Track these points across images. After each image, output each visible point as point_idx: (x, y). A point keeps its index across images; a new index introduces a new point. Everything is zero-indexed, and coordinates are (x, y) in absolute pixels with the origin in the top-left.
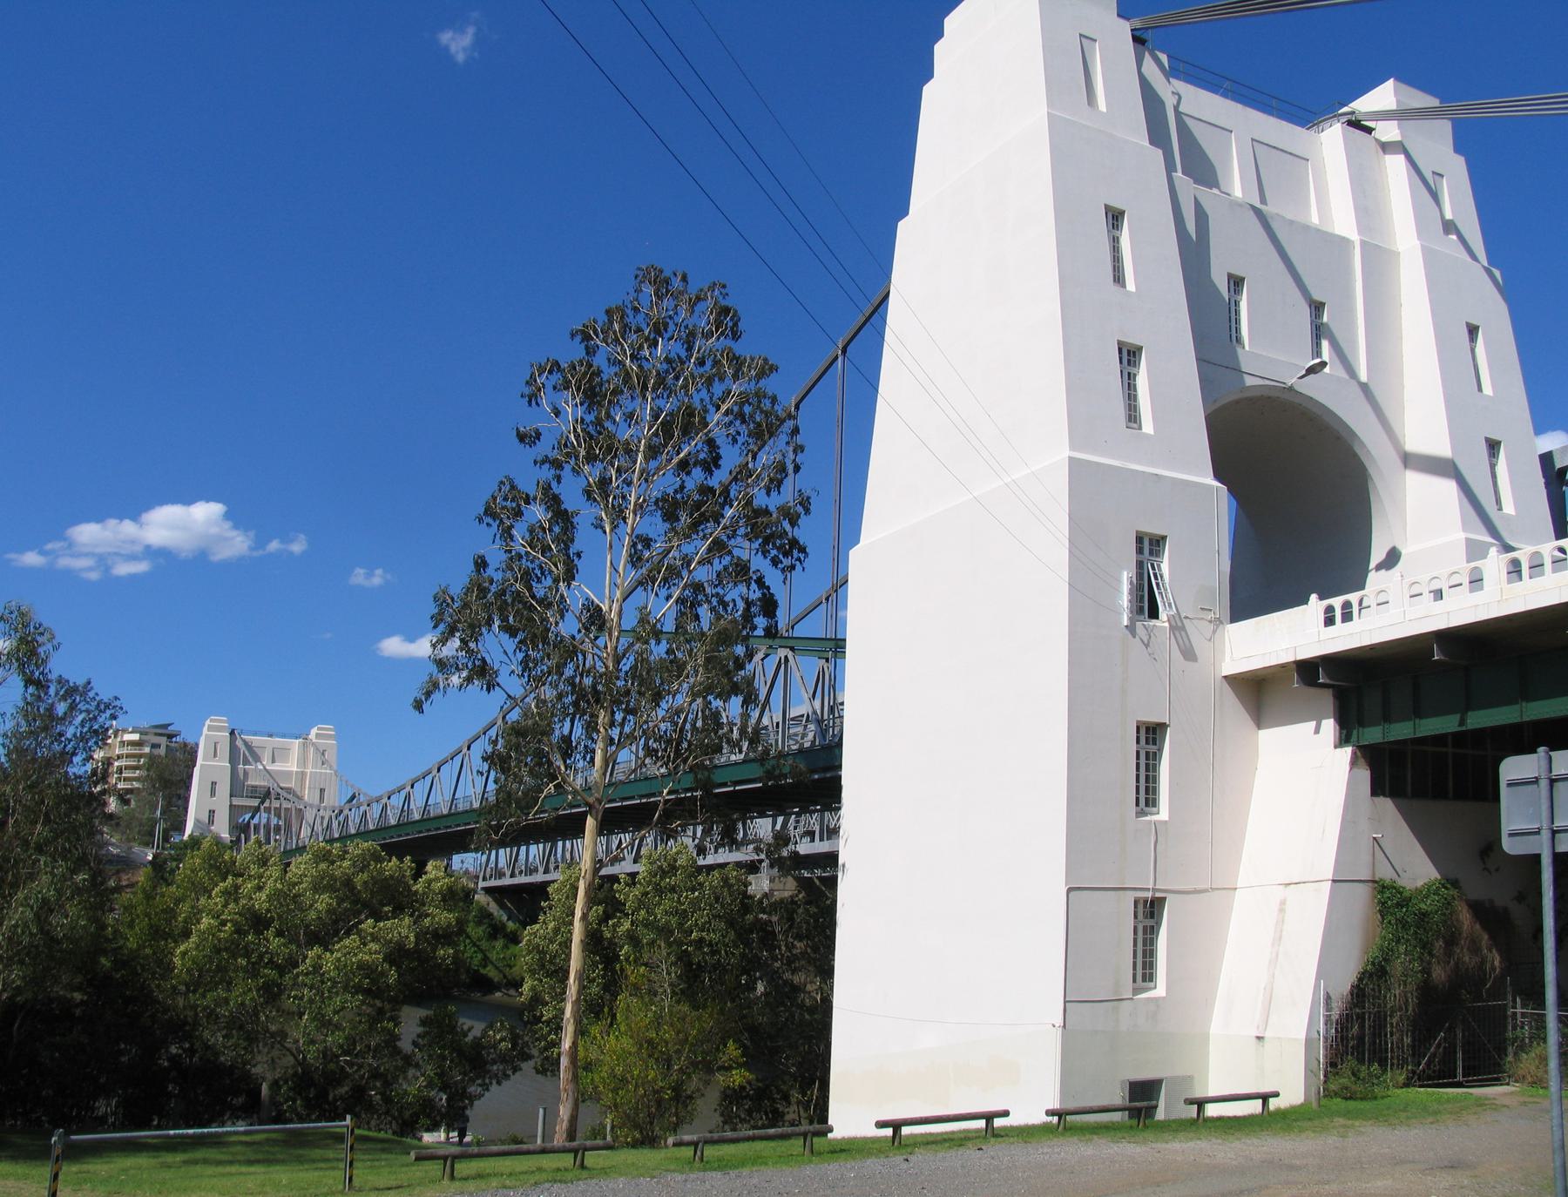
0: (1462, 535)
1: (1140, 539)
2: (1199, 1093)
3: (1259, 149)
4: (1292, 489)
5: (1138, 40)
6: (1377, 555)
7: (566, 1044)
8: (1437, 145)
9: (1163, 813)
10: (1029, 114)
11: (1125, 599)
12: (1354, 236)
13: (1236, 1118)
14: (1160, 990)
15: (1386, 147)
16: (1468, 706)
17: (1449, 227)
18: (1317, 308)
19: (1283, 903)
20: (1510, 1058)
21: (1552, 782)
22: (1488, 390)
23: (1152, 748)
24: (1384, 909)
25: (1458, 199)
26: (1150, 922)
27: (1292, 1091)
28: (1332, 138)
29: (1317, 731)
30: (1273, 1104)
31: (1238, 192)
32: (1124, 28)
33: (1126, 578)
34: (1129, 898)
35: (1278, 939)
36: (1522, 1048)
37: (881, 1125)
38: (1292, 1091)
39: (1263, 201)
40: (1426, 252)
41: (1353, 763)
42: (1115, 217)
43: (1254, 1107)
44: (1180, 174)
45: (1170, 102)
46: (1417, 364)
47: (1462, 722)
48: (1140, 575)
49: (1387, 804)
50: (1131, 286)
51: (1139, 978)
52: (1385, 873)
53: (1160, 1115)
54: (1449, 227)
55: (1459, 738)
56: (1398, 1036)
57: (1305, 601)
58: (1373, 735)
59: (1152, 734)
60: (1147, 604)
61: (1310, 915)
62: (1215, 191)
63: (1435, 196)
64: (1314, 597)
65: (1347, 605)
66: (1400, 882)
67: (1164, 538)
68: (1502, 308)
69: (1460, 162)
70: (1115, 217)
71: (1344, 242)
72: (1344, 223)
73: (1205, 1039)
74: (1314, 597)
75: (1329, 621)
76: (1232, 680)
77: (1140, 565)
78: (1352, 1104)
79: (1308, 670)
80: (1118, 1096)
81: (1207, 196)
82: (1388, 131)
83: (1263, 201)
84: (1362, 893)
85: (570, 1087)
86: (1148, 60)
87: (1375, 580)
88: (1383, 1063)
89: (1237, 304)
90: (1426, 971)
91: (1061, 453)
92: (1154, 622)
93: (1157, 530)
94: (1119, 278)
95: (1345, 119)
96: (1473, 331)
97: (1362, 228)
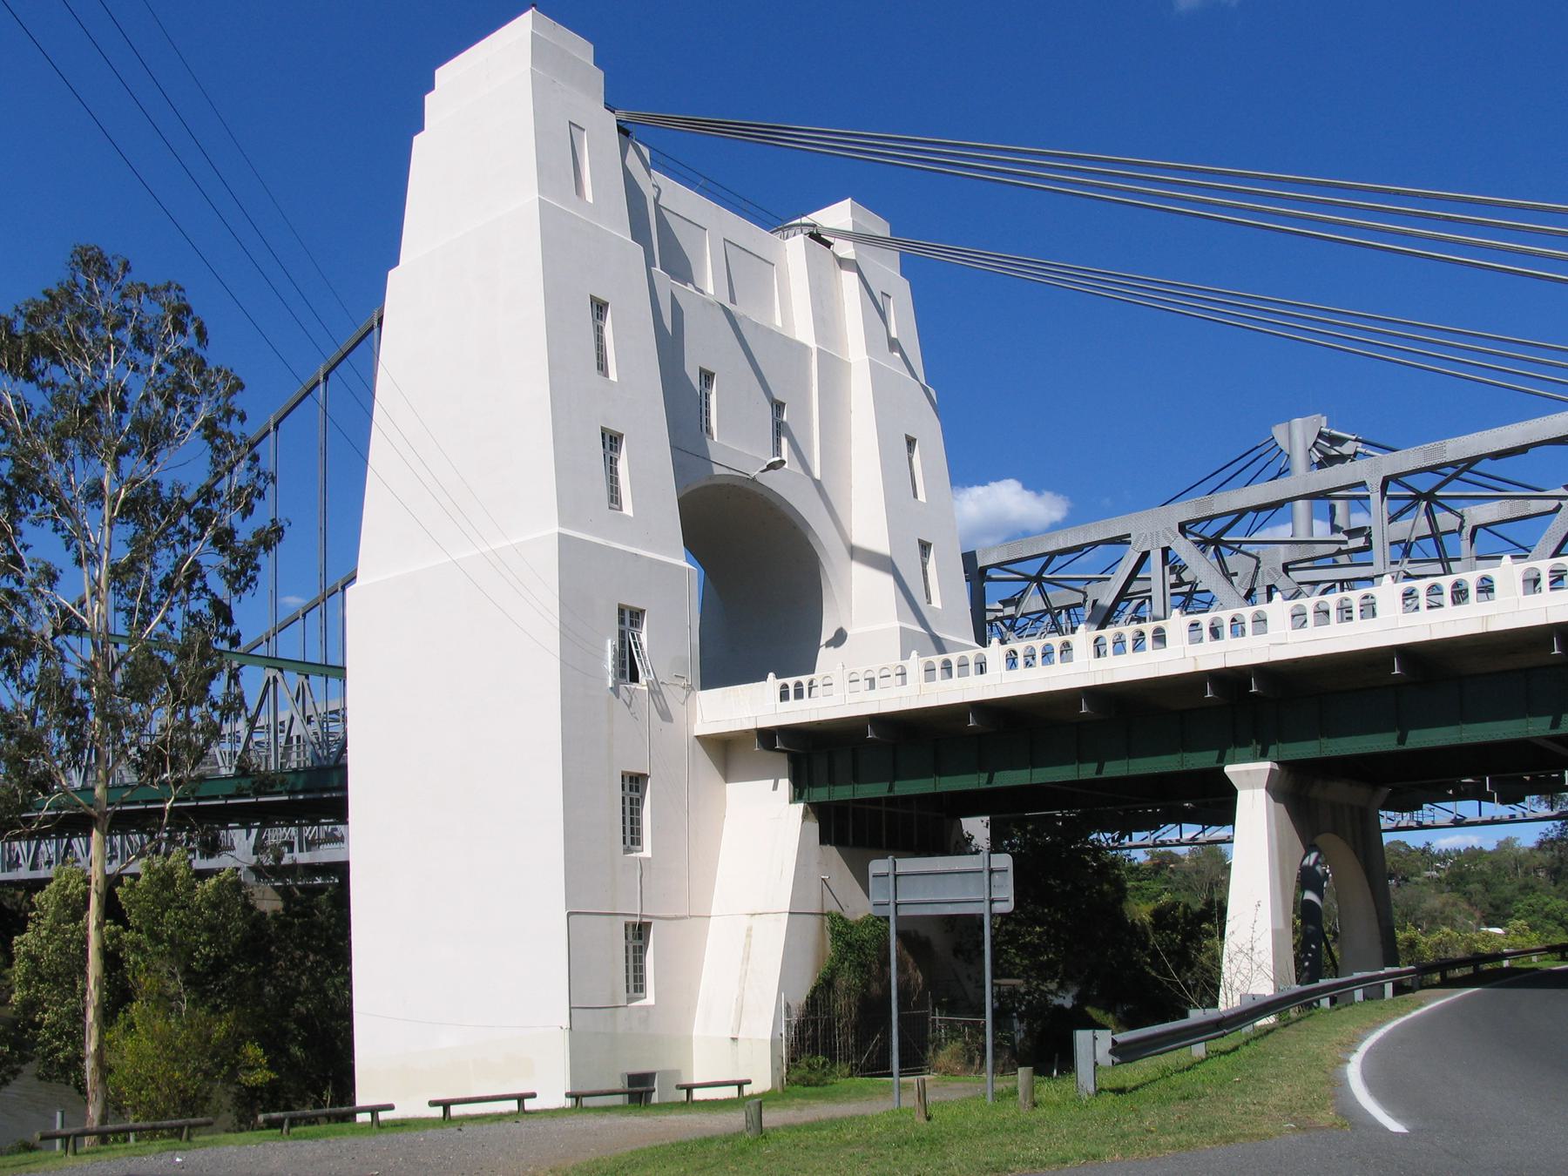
0: (897, 624)
1: (621, 611)
2: (686, 1081)
3: (731, 250)
4: (753, 572)
5: (623, 130)
6: (827, 634)
7: (91, 1047)
8: (887, 269)
9: (647, 851)
10: (522, 197)
11: (609, 664)
12: (812, 344)
13: (716, 1101)
14: (650, 999)
15: (842, 263)
16: (895, 777)
17: (894, 345)
18: (778, 407)
19: (750, 929)
20: (930, 1054)
21: (896, 876)
22: (922, 497)
23: (635, 795)
24: (837, 935)
25: (902, 321)
26: (638, 943)
27: (762, 1080)
28: (795, 247)
29: (775, 788)
30: (747, 1090)
31: (710, 289)
32: (611, 120)
33: (610, 645)
34: (622, 921)
35: (747, 958)
36: (939, 1046)
37: (433, 1104)
38: (762, 1080)
39: (733, 301)
40: (874, 367)
41: (805, 817)
42: (600, 308)
43: (732, 1092)
44: (658, 269)
45: (650, 194)
46: (869, 471)
47: (891, 789)
48: (622, 643)
49: (832, 851)
50: (613, 376)
51: (632, 989)
52: (832, 907)
53: (655, 1098)
54: (894, 345)
55: (891, 801)
56: (844, 1038)
57: (765, 679)
58: (821, 794)
59: (635, 782)
60: (628, 669)
61: (772, 939)
62: (690, 288)
63: (883, 315)
64: (771, 675)
65: (799, 684)
66: (846, 915)
67: (643, 611)
68: (935, 425)
69: (904, 285)
70: (600, 308)
71: (804, 348)
72: (804, 332)
73: (689, 1039)
74: (771, 675)
75: (784, 696)
76: (703, 740)
77: (622, 634)
78: (808, 1089)
79: (767, 737)
80: (620, 1084)
81: (684, 291)
82: (845, 249)
83: (733, 301)
84: (813, 922)
85: (99, 1088)
86: (631, 152)
87: (825, 656)
88: (833, 1058)
89: (707, 396)
90: (866, 986)
91: (552, 529)
92: (634, 685)
93: (638, 605)
94: (602, 366)
95: (806, 230)
96: (911, 442)
97: (819, 337)
